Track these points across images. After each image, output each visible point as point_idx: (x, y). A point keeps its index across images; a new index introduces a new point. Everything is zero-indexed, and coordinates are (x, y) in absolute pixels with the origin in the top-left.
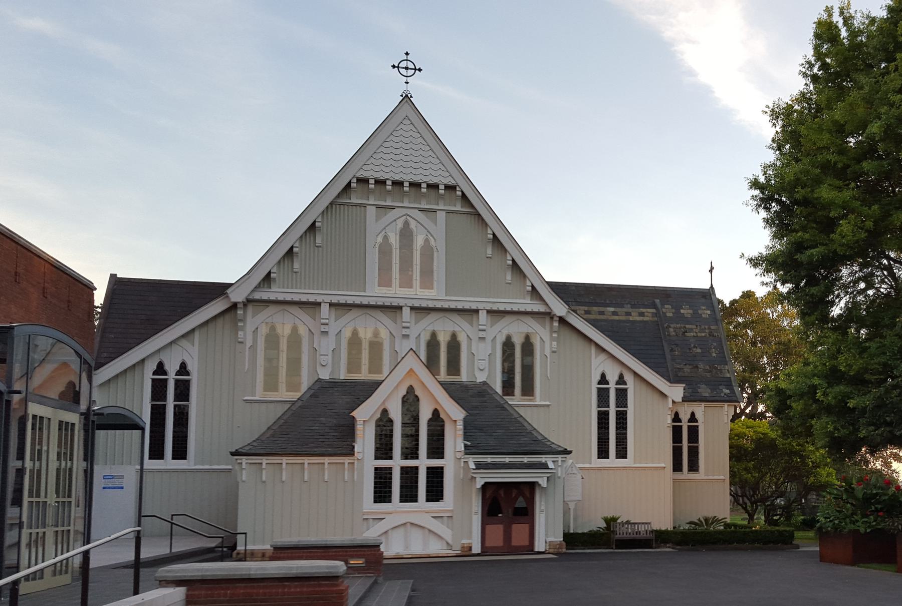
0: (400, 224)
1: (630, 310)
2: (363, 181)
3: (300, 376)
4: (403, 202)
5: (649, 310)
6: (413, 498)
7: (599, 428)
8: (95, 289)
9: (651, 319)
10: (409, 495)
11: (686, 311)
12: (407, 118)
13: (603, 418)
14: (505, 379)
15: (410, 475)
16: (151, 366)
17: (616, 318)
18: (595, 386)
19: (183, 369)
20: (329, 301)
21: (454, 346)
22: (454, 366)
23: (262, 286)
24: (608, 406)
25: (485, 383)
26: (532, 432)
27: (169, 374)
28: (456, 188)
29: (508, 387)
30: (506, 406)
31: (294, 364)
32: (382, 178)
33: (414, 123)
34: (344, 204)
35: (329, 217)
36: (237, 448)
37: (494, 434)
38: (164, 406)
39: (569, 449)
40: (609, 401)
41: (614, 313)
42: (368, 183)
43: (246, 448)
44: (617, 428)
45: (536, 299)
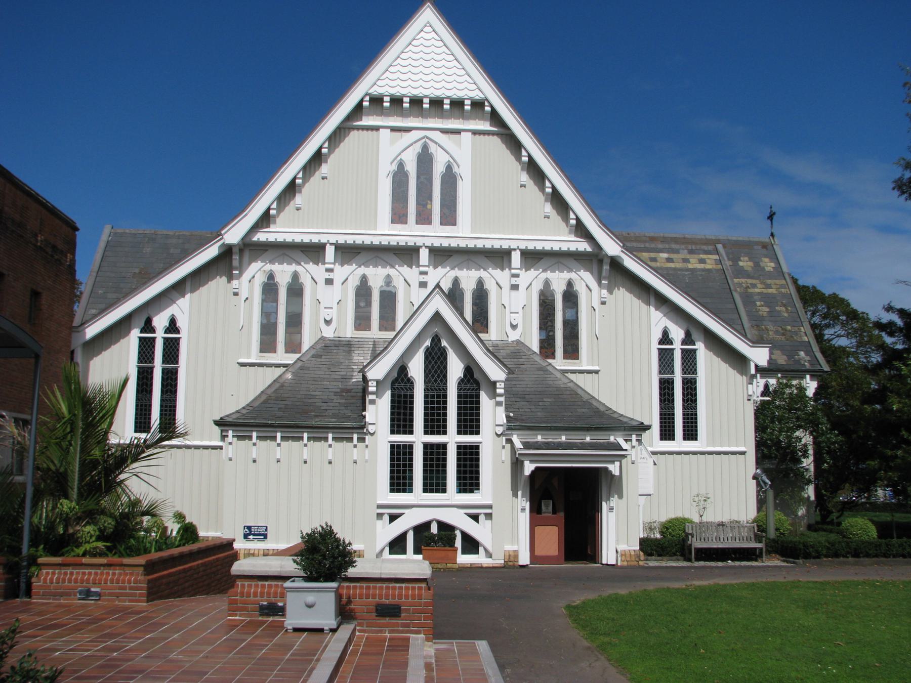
0: (418, 148)
1: (688, 256)
2: (376, 100)
3: (300, 333)
5: (710, 256)
6: (441, 488)
7: (661, 400)
8: (77, 229)
9: (714, 267)
10: (434, 483)
11: (745, 263)
12: (428, 25)
13: (666, 387)
14: (543, 338)
15: (435, 455)
17: (672, 265)
18: (655, 346)
19: (173, 327)
23: (260, 225)
24: (673, 372)
25: (518, 342)
26: (590, 401)
29: (547, 347)
30: (549, 368)
31: (295, 321)
32: (398, 94)
36: (222, 416)
37: (540, 404)
38: (152, 369)
39: (646, 423)
40: (673, 366)
41: (669, 260)
43: (234, 416)
44: (684, 400)
45: (581, 237)
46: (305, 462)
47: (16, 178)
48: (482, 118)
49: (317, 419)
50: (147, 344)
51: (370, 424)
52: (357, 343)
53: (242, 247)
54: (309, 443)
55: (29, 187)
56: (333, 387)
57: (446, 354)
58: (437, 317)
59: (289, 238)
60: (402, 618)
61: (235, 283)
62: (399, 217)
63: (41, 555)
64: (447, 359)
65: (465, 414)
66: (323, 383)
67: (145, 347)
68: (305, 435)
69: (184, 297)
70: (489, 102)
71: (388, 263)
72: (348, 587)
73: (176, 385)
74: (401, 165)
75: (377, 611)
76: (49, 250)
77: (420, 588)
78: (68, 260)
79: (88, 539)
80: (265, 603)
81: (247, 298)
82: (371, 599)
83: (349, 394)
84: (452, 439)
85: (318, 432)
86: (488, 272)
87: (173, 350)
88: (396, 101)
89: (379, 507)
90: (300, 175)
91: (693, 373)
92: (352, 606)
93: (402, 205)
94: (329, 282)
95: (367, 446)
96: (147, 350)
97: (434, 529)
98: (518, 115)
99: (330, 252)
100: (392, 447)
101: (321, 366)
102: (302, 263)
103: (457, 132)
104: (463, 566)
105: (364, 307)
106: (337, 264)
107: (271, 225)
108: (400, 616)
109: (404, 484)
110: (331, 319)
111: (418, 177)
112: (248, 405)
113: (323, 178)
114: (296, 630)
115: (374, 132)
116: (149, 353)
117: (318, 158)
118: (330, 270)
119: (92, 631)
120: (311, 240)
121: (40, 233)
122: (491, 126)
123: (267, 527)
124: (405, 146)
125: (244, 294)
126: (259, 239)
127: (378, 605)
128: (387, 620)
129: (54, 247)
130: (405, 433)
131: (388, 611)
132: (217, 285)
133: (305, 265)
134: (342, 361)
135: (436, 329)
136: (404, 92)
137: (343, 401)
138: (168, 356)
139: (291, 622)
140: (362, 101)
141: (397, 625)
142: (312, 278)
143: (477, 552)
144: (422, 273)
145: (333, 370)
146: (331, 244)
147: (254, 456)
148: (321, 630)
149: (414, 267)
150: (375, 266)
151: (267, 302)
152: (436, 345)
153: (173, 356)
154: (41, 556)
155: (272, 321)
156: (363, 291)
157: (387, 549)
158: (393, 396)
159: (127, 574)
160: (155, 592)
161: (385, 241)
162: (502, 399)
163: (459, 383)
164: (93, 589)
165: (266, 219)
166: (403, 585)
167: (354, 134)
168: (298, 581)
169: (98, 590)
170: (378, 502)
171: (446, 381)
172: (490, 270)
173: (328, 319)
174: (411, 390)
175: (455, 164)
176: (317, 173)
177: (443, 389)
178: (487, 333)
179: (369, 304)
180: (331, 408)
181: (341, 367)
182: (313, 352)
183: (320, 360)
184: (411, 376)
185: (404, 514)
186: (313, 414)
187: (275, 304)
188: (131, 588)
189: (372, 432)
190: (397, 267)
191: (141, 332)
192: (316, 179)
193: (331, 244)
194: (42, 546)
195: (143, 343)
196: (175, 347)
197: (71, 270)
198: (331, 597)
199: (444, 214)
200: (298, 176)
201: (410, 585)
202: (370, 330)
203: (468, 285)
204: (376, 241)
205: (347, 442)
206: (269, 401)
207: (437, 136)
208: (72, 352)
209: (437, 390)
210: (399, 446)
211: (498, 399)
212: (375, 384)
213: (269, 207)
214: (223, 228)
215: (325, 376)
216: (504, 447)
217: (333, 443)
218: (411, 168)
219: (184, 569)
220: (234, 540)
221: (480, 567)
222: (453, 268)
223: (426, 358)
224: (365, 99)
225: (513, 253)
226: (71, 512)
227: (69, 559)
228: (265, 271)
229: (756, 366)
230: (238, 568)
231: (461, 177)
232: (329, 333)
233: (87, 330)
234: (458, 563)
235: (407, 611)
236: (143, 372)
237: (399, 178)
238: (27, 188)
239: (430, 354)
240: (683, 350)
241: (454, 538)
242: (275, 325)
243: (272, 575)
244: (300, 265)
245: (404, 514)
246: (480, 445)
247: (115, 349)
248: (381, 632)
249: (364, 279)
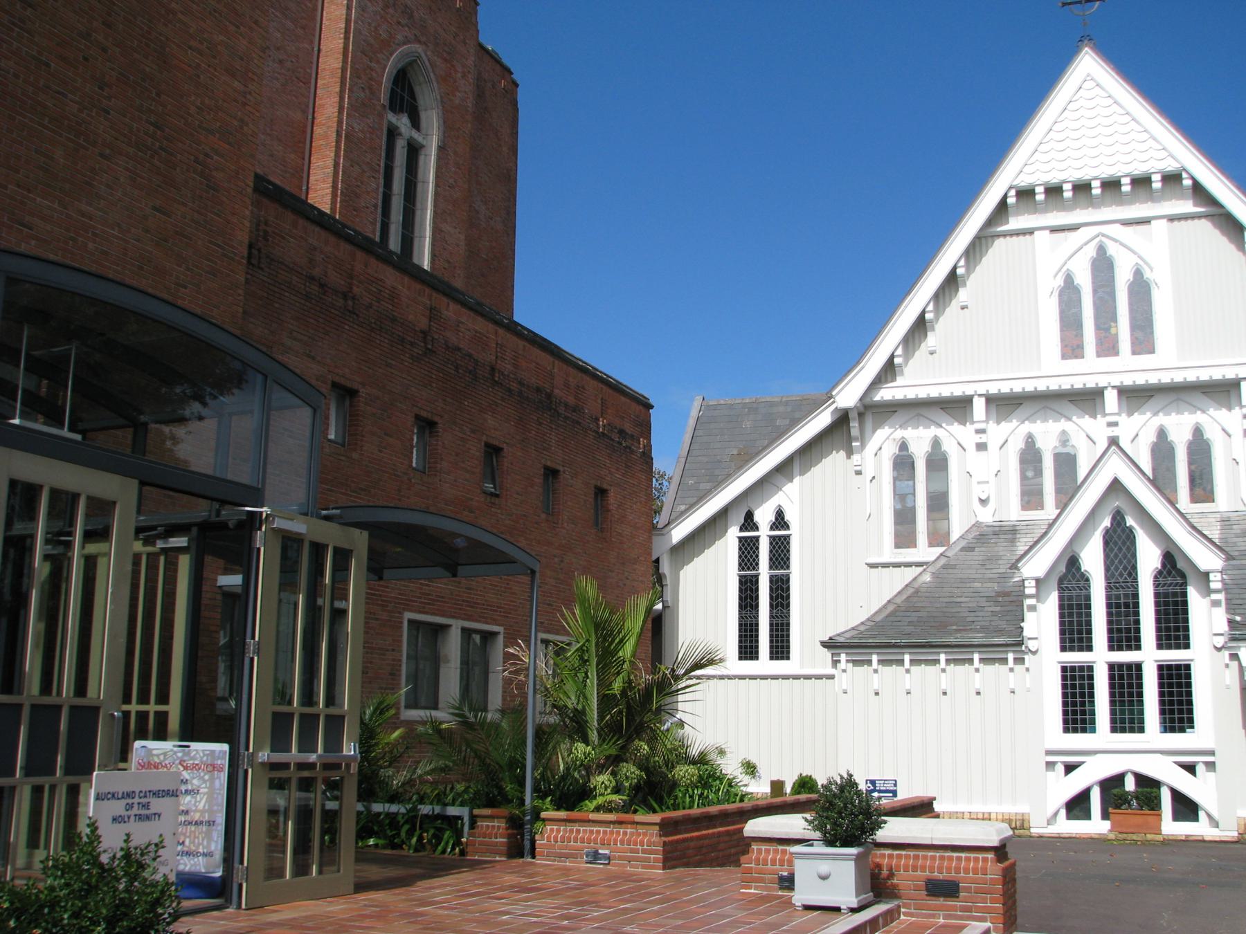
0: (1090, 251)
2: (1026, 194)
8: (652, 407)
12: (1089, 78)
19: (780, 521)
20: (985, 392)
21: (1200, 449)
22: (1202, 486)
23: (883, 379)
27: (761, 528)
28: (1181, 175)
31: (939, 503)
33: (1120, 100)
34: (999, 235)
36: (831, 635)
43: (848, 635)
46: (945, 693)
47: (565, 352)
48: (1182, 197)
49: (959, 635)
50: (749, 545)
51: (1029, 639)
52: (1025, 527)
53: (862, 409)
54: (948, 667)
55: (583, 362)
56: (986, 590)
57: (1134, 537)
58: (1116, 486)
59: (922, 393)
60: (961, 898)
61: (856, 458)
62: (1072, 349)
63: (547, 808)
64: (1135, 543)
66: (972, 585)
67: (746, 549)
68: (943, 657)
69: (792, 481)
70: (1187, 172)
71: (1061, 415)
72: (891, 856)
73: (788, 597)
74: (1069, 280)
75: (927, 889)
76: (616, 437)
77: (985, 860)
78: (641, 446)
79: (602, 791)
80: (785, 874)
81: (874, 478)
82: (919, 873)
83: (1007, 599)
85: (960, 651)
86: (1208, 415)
87: (782, 551)
88: (1054, 191)
89: (1049, 753)
90: (931, 307)
91: (754, 569)
92: (895, 881)
93: (1075, 333)
94: (981, 447)
95: (1028, 670)
96: (749, 553)
97: (1130, 785)
98: (1233, 185)
99: (979, 406)
100: (1064, 669)
101: (973, 562)
102: (944, 425)
103: (1146, 221)
104: (1174, 838)
105: (1032, 478)
106: (991, 422)
107: (898, 378)
108: (958, 897)
110: (988, 498)
111: (1095, 291)
112: (868, 619)
113: (963, 308)
114: (808, 908)
115: (1027, 237)
116: (751, 556)
117: (952, 281)
118: (980, 431)
119: (569, 897)
120: (940, 394)
121: (602, 416)
122: (1195, 205)
123: (896, 781)
124: (1069, 254)
125: (869, 472)
126: (882, 397)
127: (929, 880)
128: (941, 901)
129: (622, 432)
130: (1081, 649)
131: (943, 889)
132: (834, 462)
133: (946, 427)
134: (1001, 553)
135: (1117, 503)
137: (998, 609)
138: (777, 559)
139: (801, 896)
140: (1005, 197)
141: (954, 908)
142: (1088, 436)
143: (1195, 818)
144: (1111, 424)
145: (988, 566)
146: (980, 395)
147: (876, 687)
148: (837, 909)
149: (1099, 416)
150: (1045, 420)
151: (900, 480)
152: (1119, 524)
153: (782, 559)
154: (547, 809)
155: (909, 505)
156: (1030, 457)
157: (1063, 812)
158: (1061, 599)
159: (639, 834)
160: (674, 858)
161: (1054, 385)
162: (1221, 597)
163: (1156, 577)
164: (600, 851)
165: (889, 370)
166: (963, 855)
167: (999, 243)
168: (818, 845)
169: (607, 852)
171: (1137, 575)
172: (1211, 411)
173: (983, 498)
174: (1087, 589)
175: (1145, 267)
176: (954, 302)
177: (1133, 586)
178: (1213, 501)
179: (1039, 473)
180: (980, 619)
181: (1000, 562)
182: (963, 544)
183: (971, 553)
184: (1086, 571)
185: (1083, 762)
186: (955, 627)
187: (911, 483)
188: (644, 851)
189: (1033, 650)
190: (1074, 418)
191: (741, 530)
192: (953, 309)
193: (980, 395)
194: (549, 798)
195: (743, 545)
196: (785, 547)
197: (647, 458)
198: (850, 867)
199: (1137, 338)
200: (927, 309)
201: (972, 855)
202: (1043, 509)
203: (1180, 437)
204: (1042, 386)
205: (926, 665)
206: (897, 614)
207: (1116, 230)
208: (657, 561)
209: (1123, 588)
210: (1073, 669)
211: (1214, 597)
212: (1033, 583)
213: (893, 354)
214: (834, 387)
215: (977, 576)
216: (1227, 666)
217: (981, 666)
218: (1084, 280)
219: (727, 832)
220: (934, 799)
221: (1200, 841)
222: (1156, 414)
223: (1106, 543)
224: (1009, 194)
225: (1106, 393)
226: (586, 758)
227: (575, 814)
228: (894, 440)
230: (752, 829)
231: (1156, 284)
232: (986, 516)
233: (673, 532)
234: (1163, 833)
235: (968, 890)
236: (746, 582)
237: (1069, 294)
238: (581, 363)
239: (1112, 537)
241: (1158, 799)
242: (913, 510)
244: (941, 427)
245: (1083, 762)
246: (1095, 665)
247: (709, 553)
248: (933, 916)
249: (1030, 441)
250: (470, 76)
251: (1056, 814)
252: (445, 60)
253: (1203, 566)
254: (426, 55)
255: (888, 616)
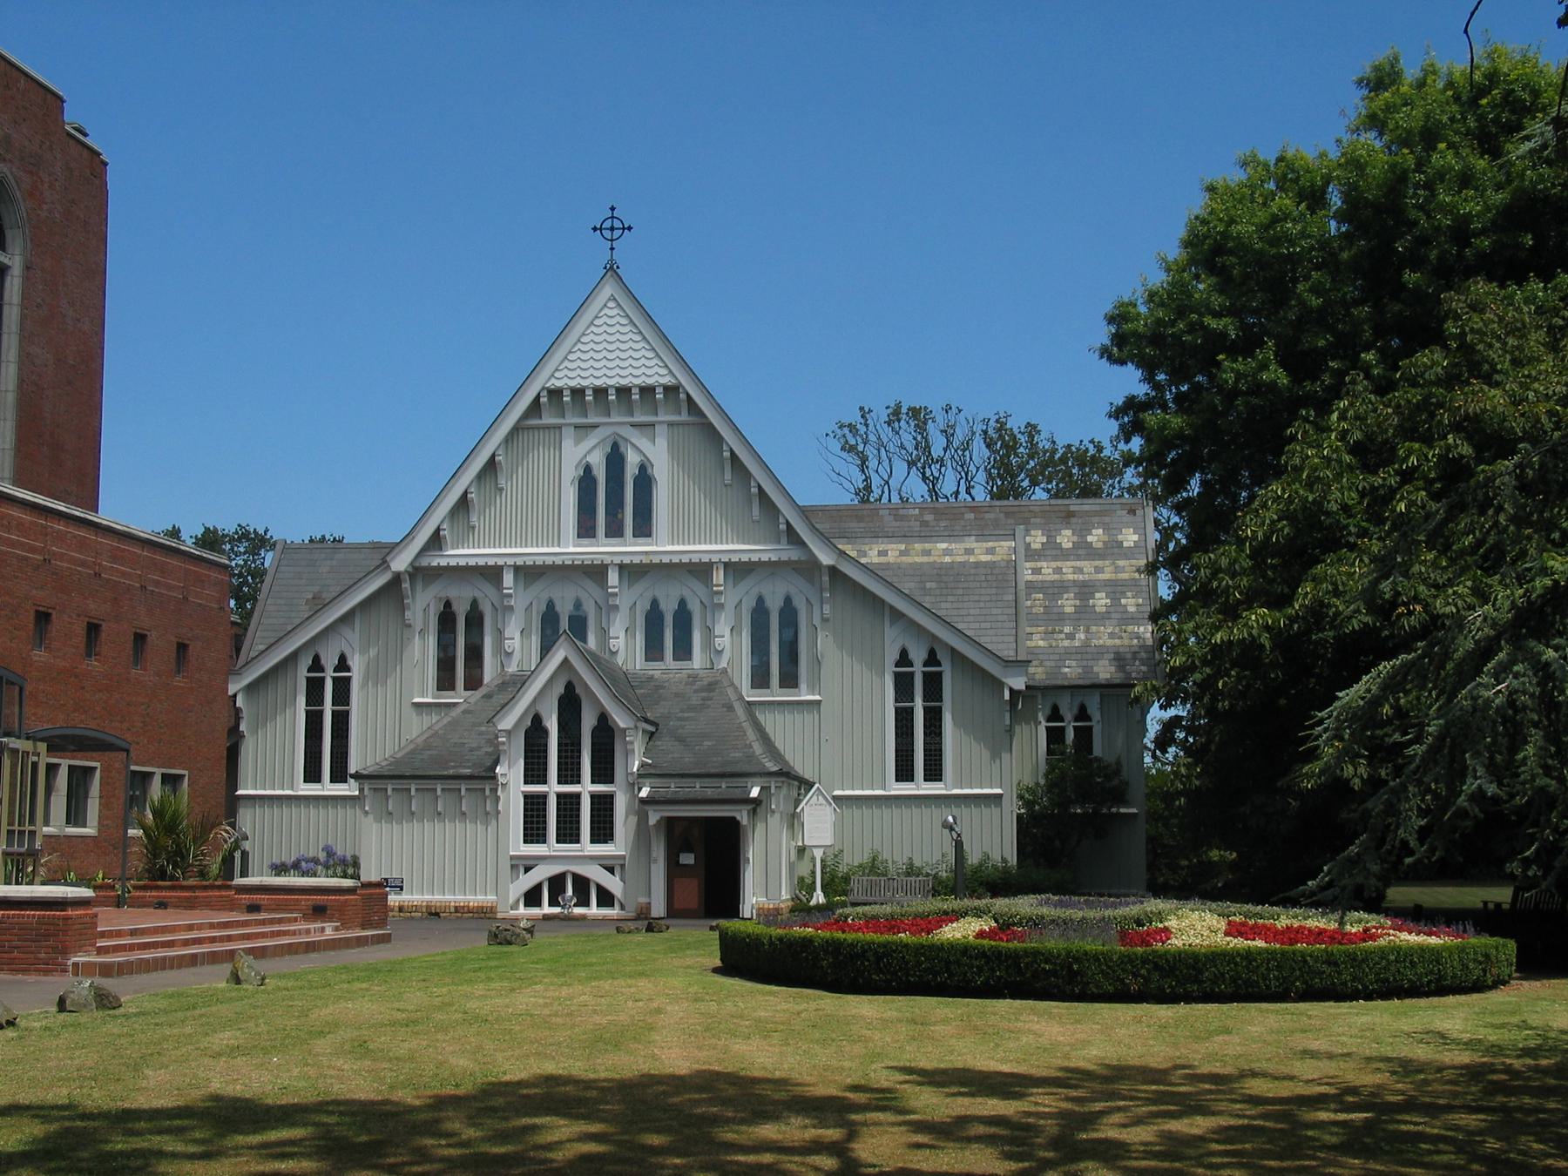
2: (555, 393)
4: (564, 417)
10: (568, 833)
13: (904, 720)
15: (569, 804)
16: (306, 662)
18: (890, 668)
31: (475, 655)
35: (515, 452)
42: (562, 396)
65: (533, 770)
74: (588, 469)
84: (586, 788)
109: (532, 835)
136: (585, 383)
140: (538, 397)
143: (612, 905)
170: (511, 853)
191: (308, 672)
218: (600, 474)
229: (1011, 690)
237: (586, 482)
240: (924, 673)
243: (1423, 1002)
249: (551, 605)
250: (57, 184)
251: (518, 901)
252: (31, 172)
253: (622, 725)
254: (12, 173)
255: (407, 754)
